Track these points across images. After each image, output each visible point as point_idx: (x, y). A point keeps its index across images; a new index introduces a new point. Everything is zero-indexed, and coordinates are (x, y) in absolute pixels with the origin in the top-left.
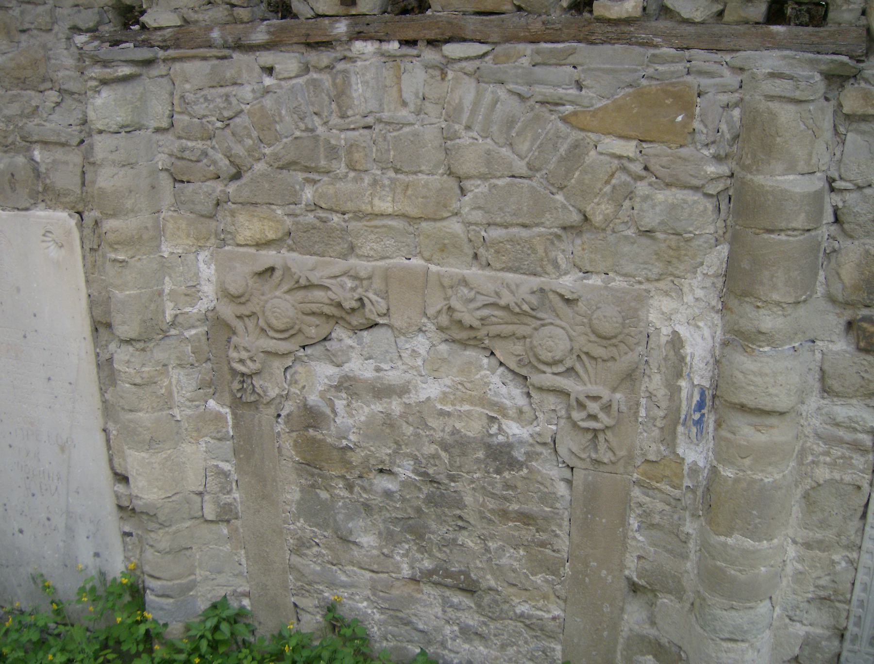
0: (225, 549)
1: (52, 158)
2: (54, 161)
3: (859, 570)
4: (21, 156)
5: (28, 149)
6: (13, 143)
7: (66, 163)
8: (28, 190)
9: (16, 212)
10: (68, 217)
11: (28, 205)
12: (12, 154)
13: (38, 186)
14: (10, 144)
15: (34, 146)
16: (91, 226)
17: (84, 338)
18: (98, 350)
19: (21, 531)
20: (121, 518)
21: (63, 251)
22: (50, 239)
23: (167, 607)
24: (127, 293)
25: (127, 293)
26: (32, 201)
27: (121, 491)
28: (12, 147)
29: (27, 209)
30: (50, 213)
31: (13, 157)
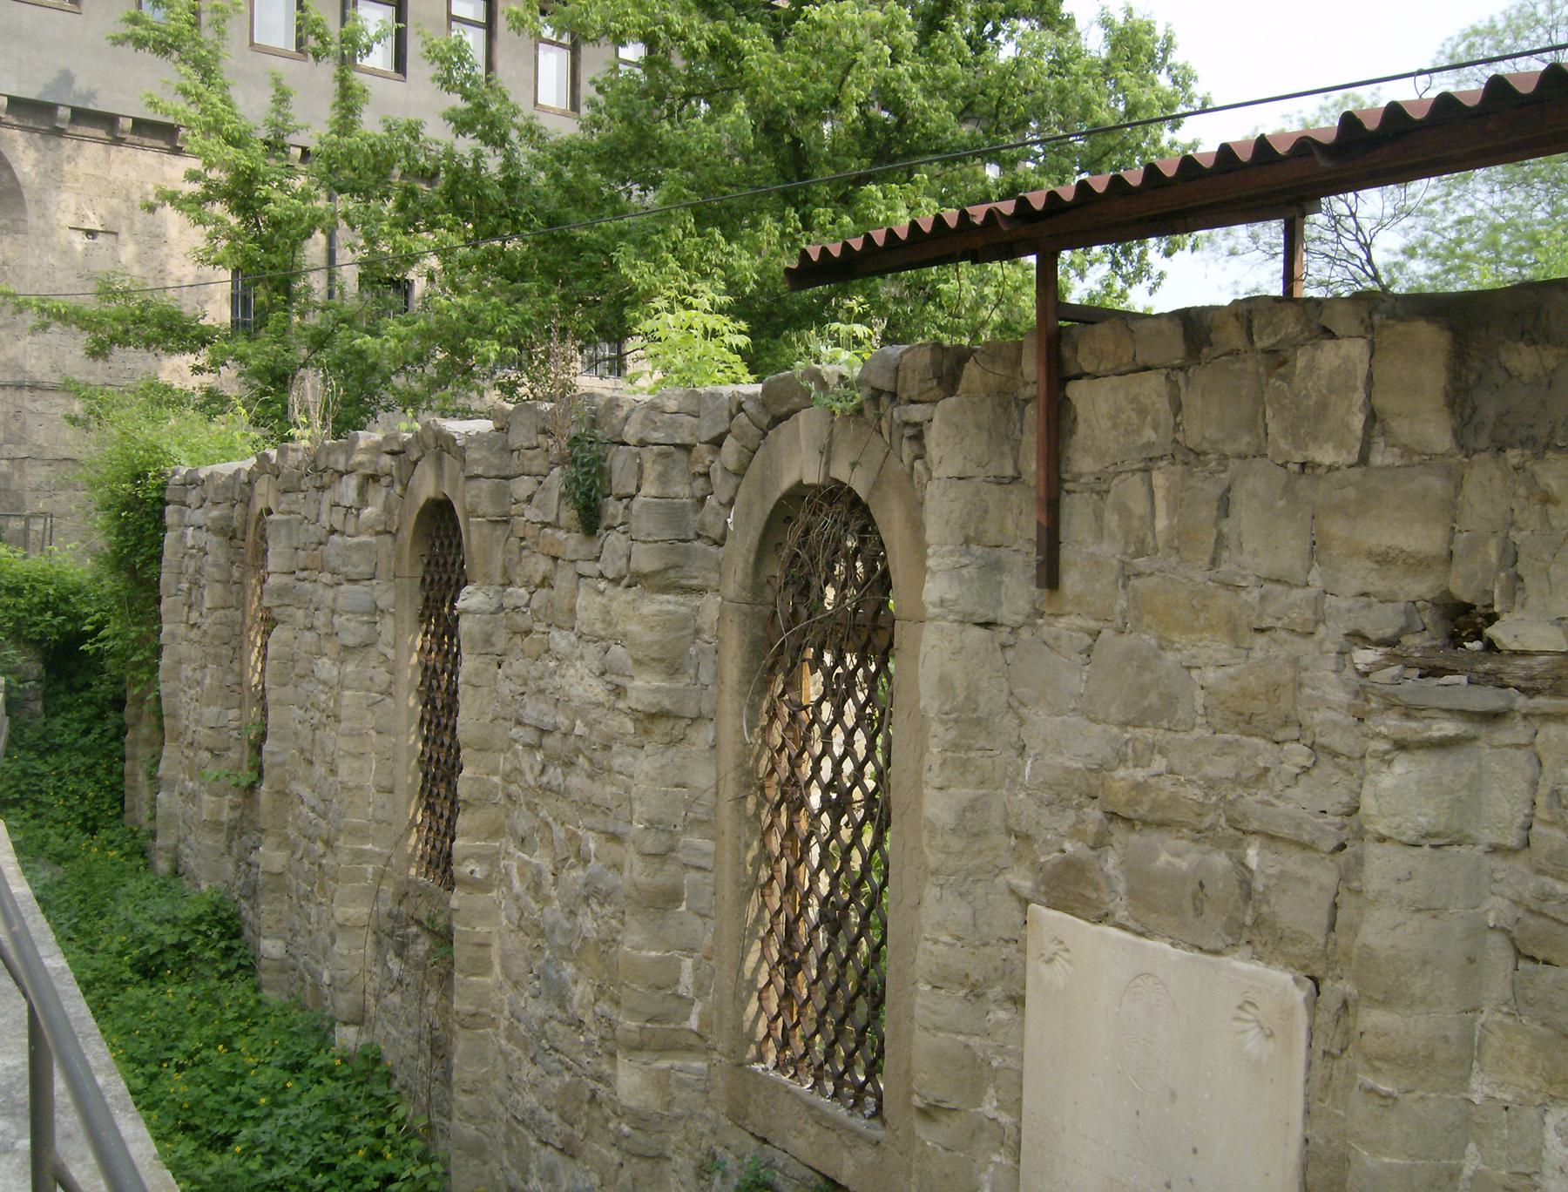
2: (1283, 875)
4: (1223, 853)
5: (1237, 844)
6: (1212, 827)
7: (1305, 881)
9: (1196, 954)
11: (1220, 945)
12: (1207, 846)
15: (1251, 838)
16: (1334, 1010)
24: (1387, 1160)
25: (1387, 1160)
26: (1230, 940)
28: (1210, 834)
30: (1257, 967)
31: (1208, 852)
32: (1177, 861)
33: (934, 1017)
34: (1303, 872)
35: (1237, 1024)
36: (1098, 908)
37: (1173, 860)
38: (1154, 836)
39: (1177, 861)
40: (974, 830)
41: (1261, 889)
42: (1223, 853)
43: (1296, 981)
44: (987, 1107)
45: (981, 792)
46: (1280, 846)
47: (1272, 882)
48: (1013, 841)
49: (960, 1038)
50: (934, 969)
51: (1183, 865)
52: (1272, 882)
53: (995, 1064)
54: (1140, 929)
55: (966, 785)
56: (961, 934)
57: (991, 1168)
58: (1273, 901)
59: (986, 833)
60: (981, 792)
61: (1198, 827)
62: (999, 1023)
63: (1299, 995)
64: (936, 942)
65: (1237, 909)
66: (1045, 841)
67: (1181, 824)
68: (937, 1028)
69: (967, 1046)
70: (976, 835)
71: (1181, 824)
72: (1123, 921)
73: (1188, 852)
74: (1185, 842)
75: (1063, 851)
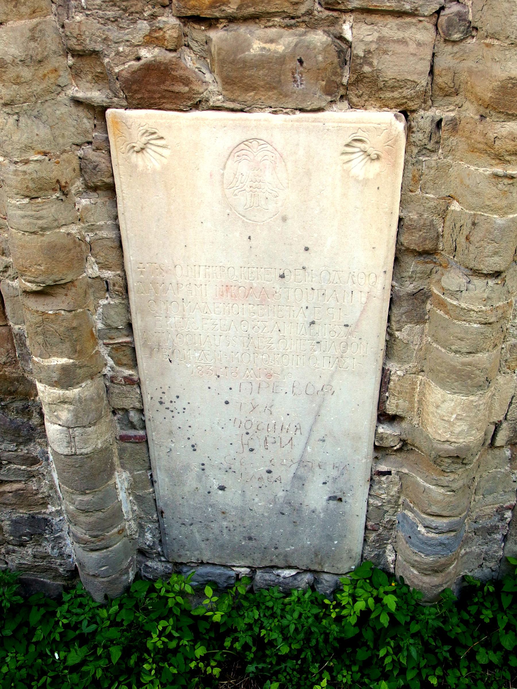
0: (503, 470)
1: (376, 35)
2: (381, 39)
3: (33, 236)
4: (320, 32)
5: (334, 22)
6: (309, 13)
7: (403, 42)
8: (324, 83)
9: (299, 115)
10: (394, 118)
11: (323, 104)
12: (302, 30)
13: (342, 76)
14: (303, 15)
15: (344, 17)
16: (428, 130)
17: (385, 272)
18: (394, 283)
19: (222, 488)
20: (376, 458)
21: (377, 165)
22: (358, 150)
23: (446, 542)
24: (511, 216)
25: (511, 216)
26: (329, 98)
27: (388, 432)
28: (306, 19)
29: (320, 110)
30: (359, 114)
31: (305, 34)
32: (272, 47)
33: (40, 222)
34: (400, 35)
35: (346, 158)
36: (190, 99)
37: (267, 46)
38: (243, 30)
39: (272, 47)
40: (39, 58)
41: (362, 54)
42: (320, 32)
43: (396, 116)
44: (90, 271)
45: (35, 21)
46: (375, 18)
47: (373, 47)
48: (71, 61)
49: (63, 230)
50: (31, 185)
51: (280, 48)
52: (373, 47)
53: (88, 239)
54: (238, 106)
55: (21, 17)
56: (47, 149)
57: (100, 310)
58: (375, 62)
59: (46, 57)
60: (35, 21)
61: (293, 14)
62: (86, 208)
63: (400, 126)
64: (27, 162)
65: (335, 74)
66: (118, 53)
67: (271, 15)
68: (43, 229)
69: (68, 234)
70: (40, 62)
71: (271, 15)
72: (219, 104)
73: (281, 37)
74: (274, 30)
75: (138, 59)
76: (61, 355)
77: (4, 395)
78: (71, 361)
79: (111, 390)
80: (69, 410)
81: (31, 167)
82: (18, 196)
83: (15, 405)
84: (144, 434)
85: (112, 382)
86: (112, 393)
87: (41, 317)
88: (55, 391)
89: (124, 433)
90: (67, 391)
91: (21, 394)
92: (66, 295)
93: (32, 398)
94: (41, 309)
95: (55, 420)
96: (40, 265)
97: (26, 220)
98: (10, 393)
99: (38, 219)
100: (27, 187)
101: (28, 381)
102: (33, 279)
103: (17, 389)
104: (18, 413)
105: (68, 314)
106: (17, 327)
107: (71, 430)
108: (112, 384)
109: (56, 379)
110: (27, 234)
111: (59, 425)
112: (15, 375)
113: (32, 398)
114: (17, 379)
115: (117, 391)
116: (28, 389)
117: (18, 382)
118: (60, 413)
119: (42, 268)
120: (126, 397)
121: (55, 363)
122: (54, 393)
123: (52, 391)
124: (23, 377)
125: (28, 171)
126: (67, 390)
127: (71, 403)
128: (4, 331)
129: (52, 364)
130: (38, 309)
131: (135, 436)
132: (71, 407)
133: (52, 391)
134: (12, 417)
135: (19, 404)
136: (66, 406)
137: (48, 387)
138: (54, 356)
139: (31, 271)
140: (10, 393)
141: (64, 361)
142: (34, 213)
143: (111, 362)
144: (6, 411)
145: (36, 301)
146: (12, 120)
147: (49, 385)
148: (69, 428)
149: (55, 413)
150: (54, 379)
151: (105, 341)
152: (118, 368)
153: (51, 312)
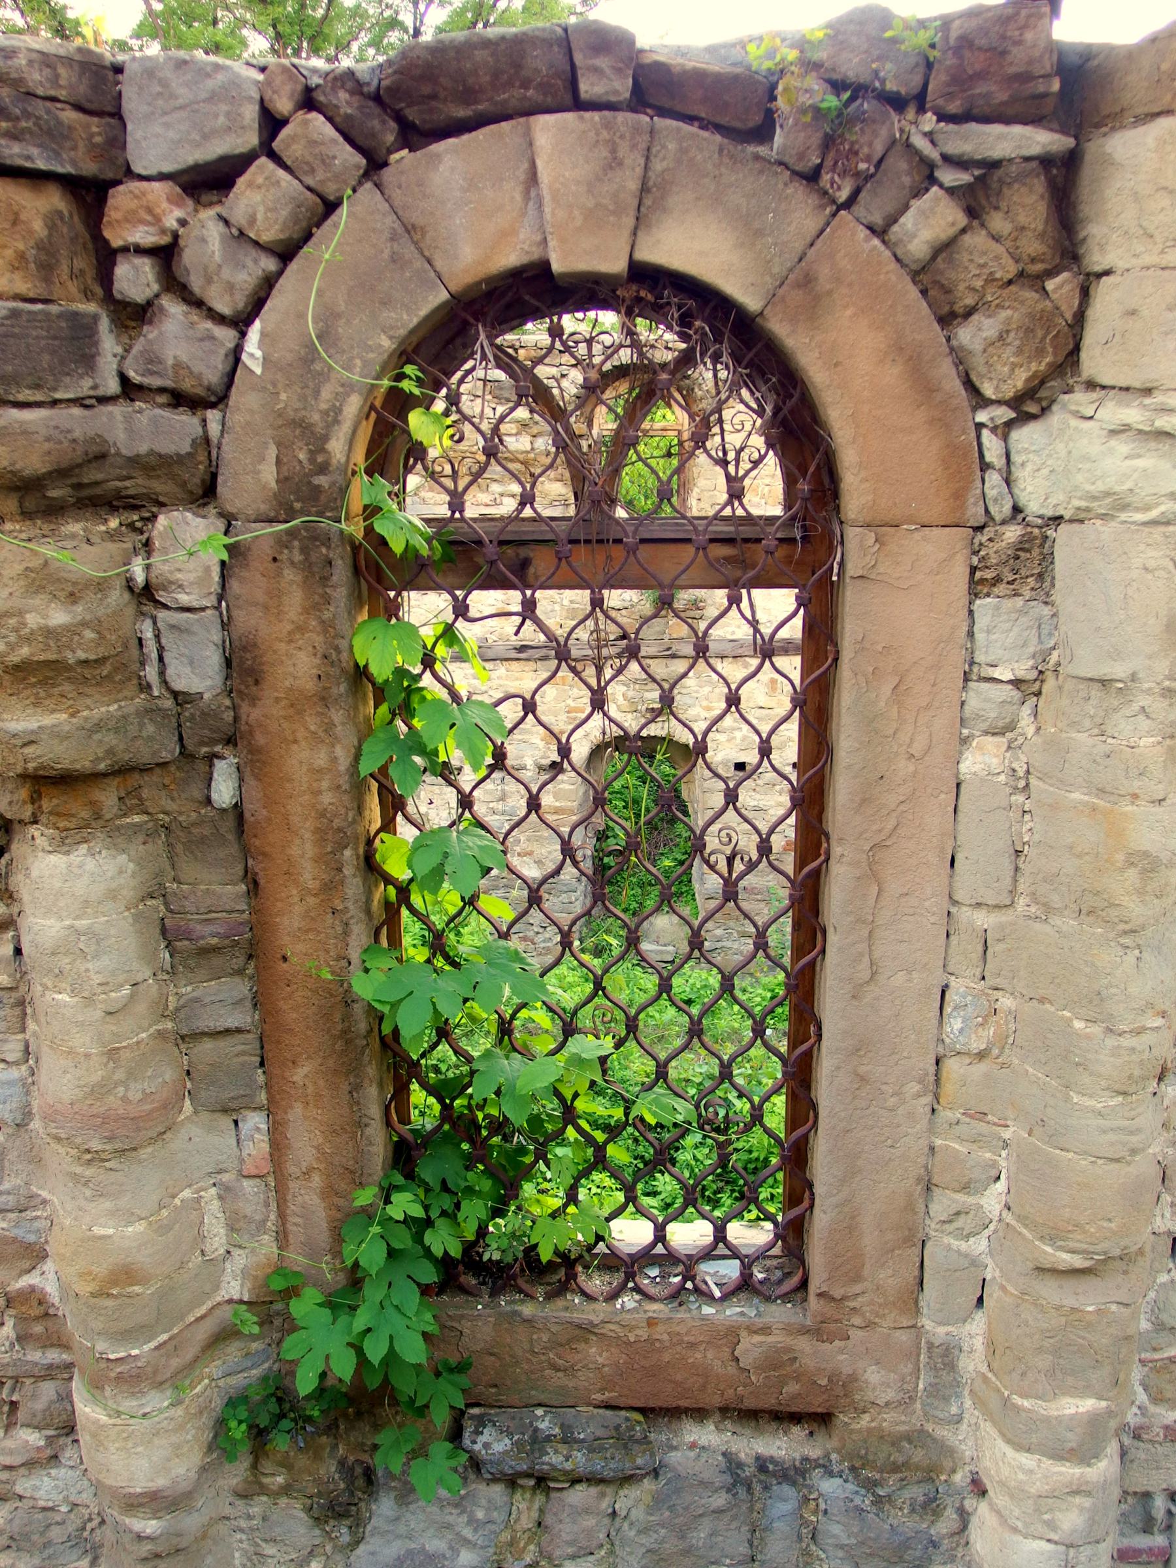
3: (1116, 1166)
76: (1085, 1391)
77: (881, 1472)
78: (1104, 1404)
79: (1132, 1454)
80: (1082, 1509)
81: (1147, 1039)
82: (1107, 1093)
83: (907, 1494)
84: (1166, 1543)
85: (1137, 1437)
86: (1132, 1461)
87: (1063, 1319)
88: (1063, 1469)
89: (1126, 1542)
90: (1089, 1470)
91: (918, 1468)
92: (1125, 1272)
93: (943, 1478)
94: (1070, 1301)
95: (1040, 1529)
96: (1110, 1220)
97: (1112, 1137)
98: (895, 1468)
99: (1131, 1133)
100: (1130, 1077)
101: (934, 1440)
102: (1085, 1246)
103: (910, 1458)
104: (913, 1511)
105: (1123, 1309)
106: (942, 1330)
107: (1072, 1552)
108: (1136, 1443)
109: (1073, 1445)
110: (1100, 1162)
111: (1049, 1541)
112: (902, 1428)
113: (943, 1478)
114: (908, 1438)
115: (1143, 1456)
116: (934, 1458)
117: (910, 1442)
118: (1059, 1515)
119: (1113, 1225)
120: (1157, 1468)
121: (1072, 1411)
122: (1061, 1474)
123: (1057, 1469)
124: (922, 1431)
125: (1139, 1048)
126: (1089, 1465)
127: (1088, 1494)
128: (904, 1338)
129: (1067, 1412)
130: (1065, 1302)
131: (1150, 1549)
132: (1087, 1502)
133: (1057, 1469)
134: (895, 1522)
135: (917, 1492)
136: (1078, 1500)
137: (1047, 1463)
138: (1063, 1394)
139: (1085, 1232)
140: (895, 1468)
141: (1088, 1405)
142: (1127, 1123)
143: (1142, 1397)
144: (887, 1507)
145: (1061, 1287)
146: (1131, 958)
147: (1051, 1457)
148: (1069, 1546)
149: (1046, 1517)
150: (1069, 1445)
151: (1143, 1356)
152: (1152, 1409)
153: (1090, 1309)
